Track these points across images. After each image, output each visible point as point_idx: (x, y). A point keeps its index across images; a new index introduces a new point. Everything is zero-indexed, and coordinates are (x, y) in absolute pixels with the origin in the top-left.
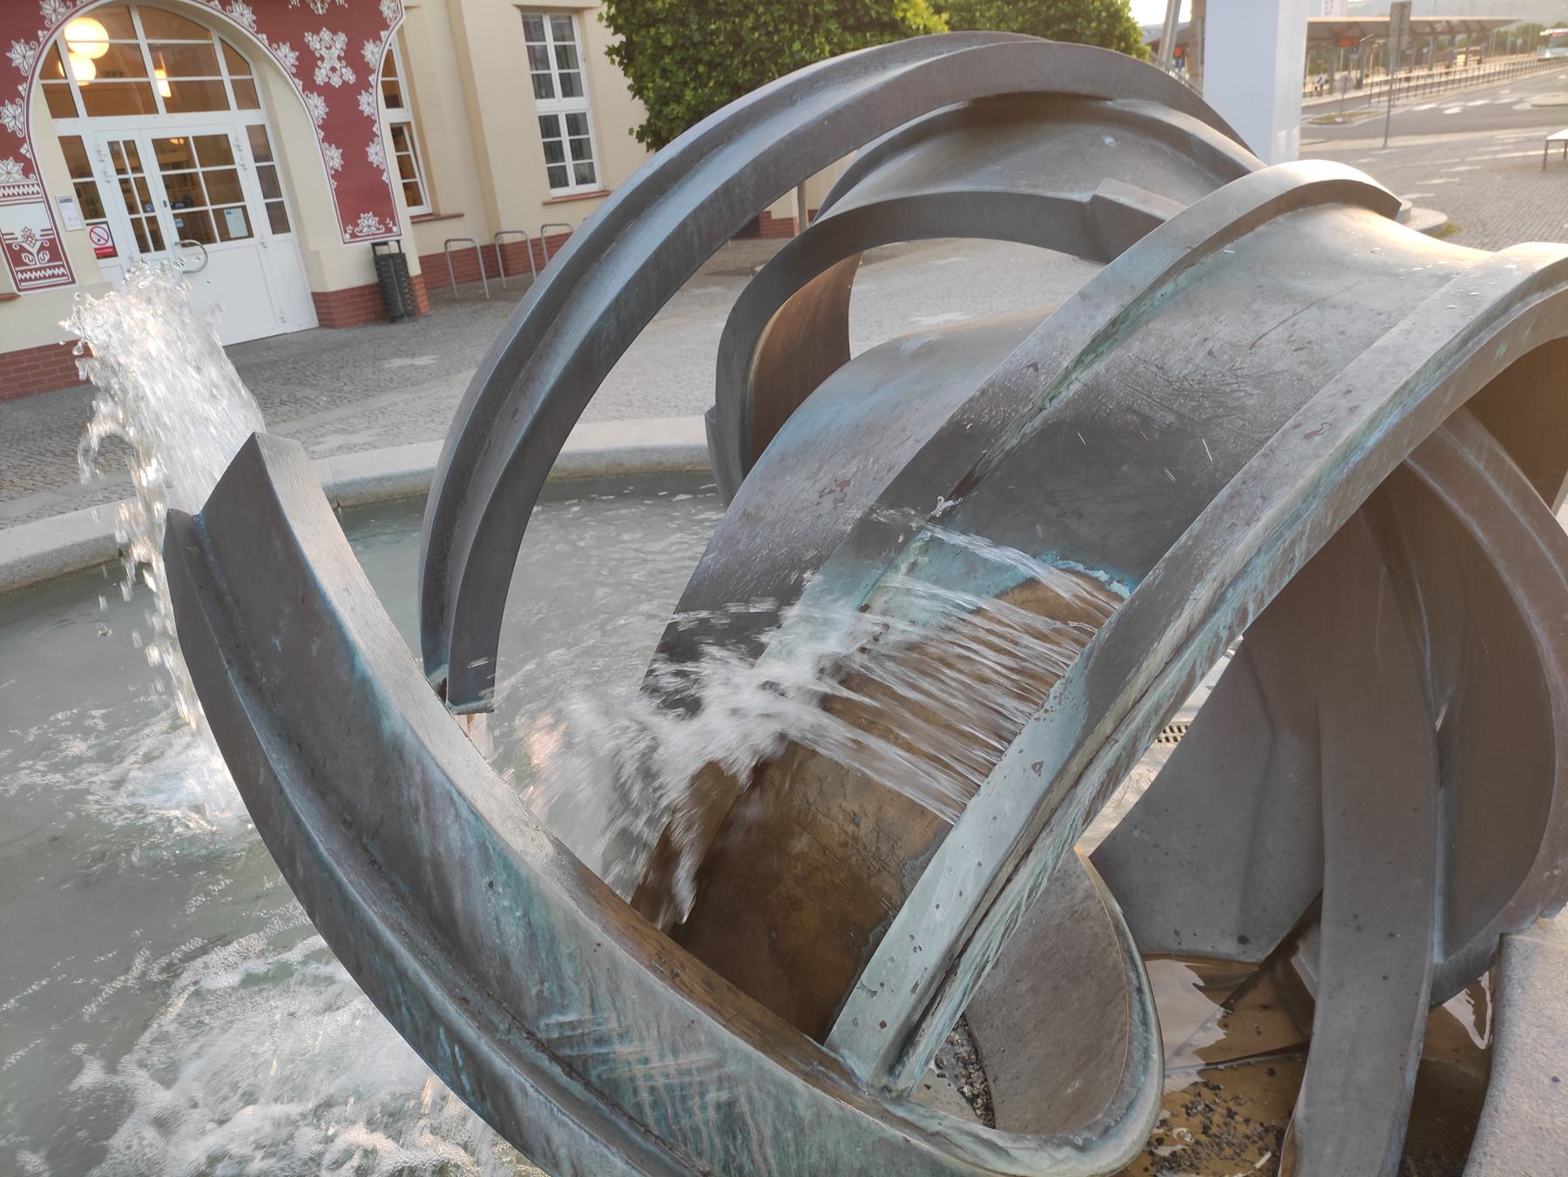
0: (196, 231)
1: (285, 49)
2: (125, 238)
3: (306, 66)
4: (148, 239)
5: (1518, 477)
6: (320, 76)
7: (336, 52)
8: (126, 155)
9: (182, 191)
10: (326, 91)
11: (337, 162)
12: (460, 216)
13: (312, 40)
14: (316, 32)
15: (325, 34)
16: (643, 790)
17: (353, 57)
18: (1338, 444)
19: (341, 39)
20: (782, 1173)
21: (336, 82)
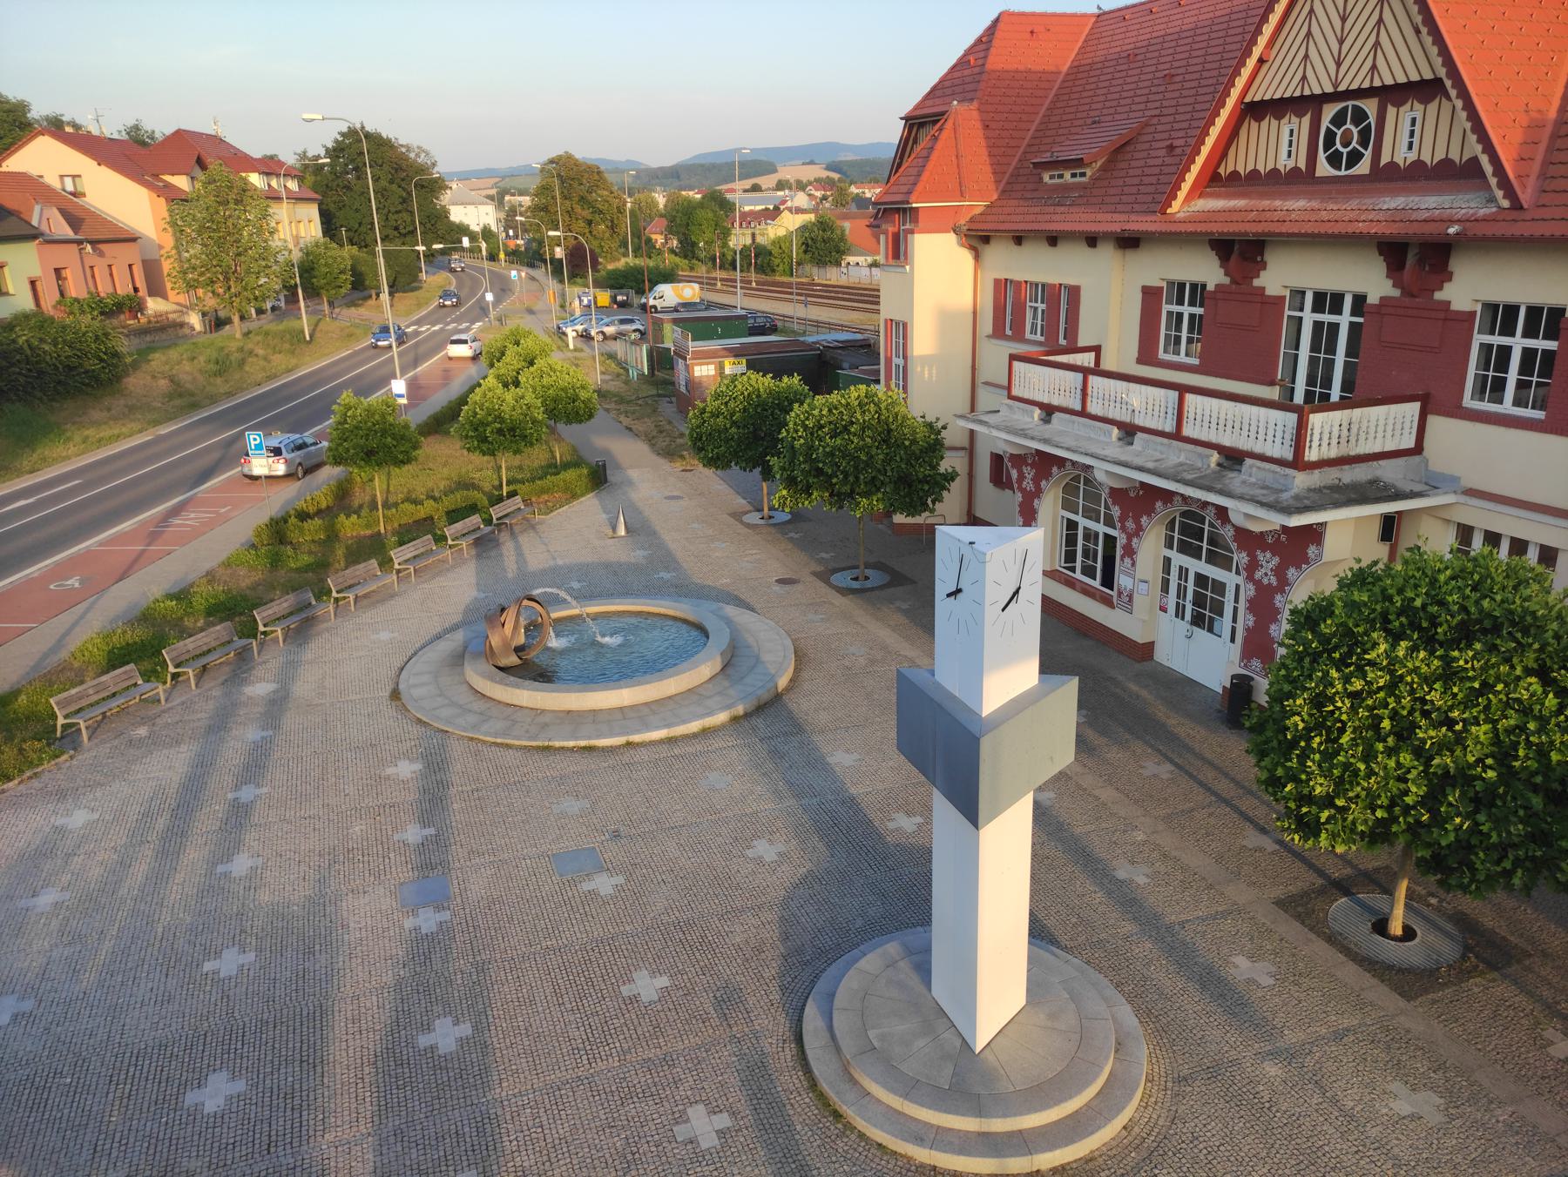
0: (1198, 621)
1: (1244, 554)
2: (1172, 608)
3: (1253, 566)
4: (1180, 612)
5: (57, 564)
6: (1258, 575)
7: (1270, 566)
8: (1183, 572)
9: (1199, 601)
10: (1258, 583)
11: (1251, 624)
12: (949, 595)
13: (1260, 556)
14: (1264, 551)
15: (1268, 555)
16: (669, 277)
17: (1280, 572)
18: (1315, 204)
19: (1276, 560)
20: (3, 791)
21: (1265, 581)
